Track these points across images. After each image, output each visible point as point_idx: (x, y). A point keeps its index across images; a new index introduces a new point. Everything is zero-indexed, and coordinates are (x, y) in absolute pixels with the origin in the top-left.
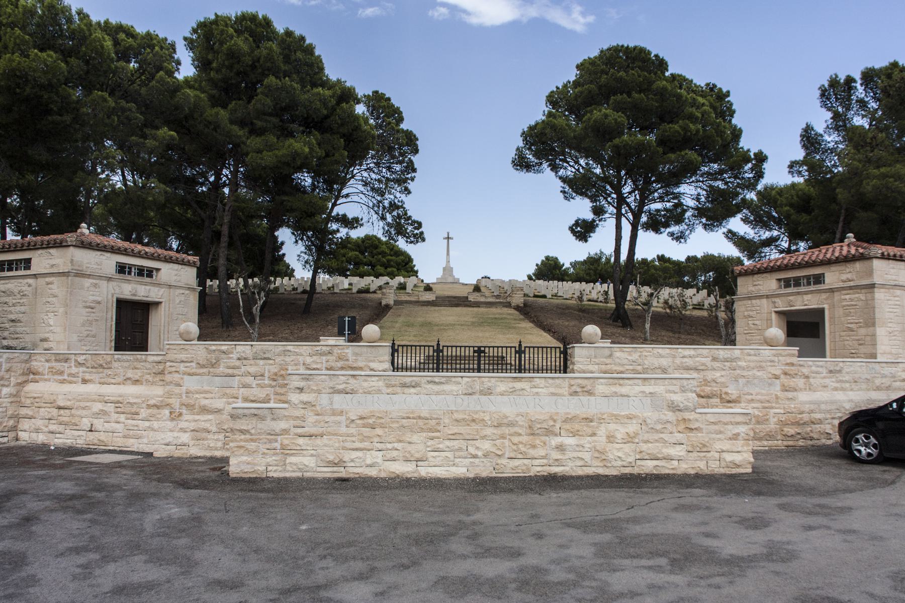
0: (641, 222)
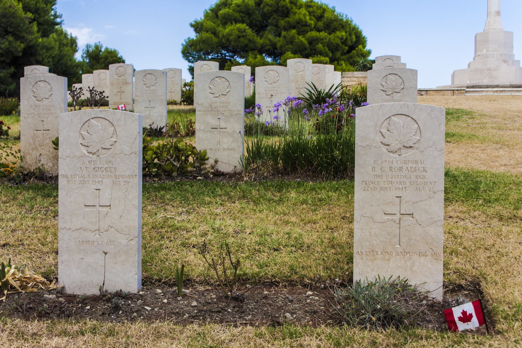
0: (456, 319)
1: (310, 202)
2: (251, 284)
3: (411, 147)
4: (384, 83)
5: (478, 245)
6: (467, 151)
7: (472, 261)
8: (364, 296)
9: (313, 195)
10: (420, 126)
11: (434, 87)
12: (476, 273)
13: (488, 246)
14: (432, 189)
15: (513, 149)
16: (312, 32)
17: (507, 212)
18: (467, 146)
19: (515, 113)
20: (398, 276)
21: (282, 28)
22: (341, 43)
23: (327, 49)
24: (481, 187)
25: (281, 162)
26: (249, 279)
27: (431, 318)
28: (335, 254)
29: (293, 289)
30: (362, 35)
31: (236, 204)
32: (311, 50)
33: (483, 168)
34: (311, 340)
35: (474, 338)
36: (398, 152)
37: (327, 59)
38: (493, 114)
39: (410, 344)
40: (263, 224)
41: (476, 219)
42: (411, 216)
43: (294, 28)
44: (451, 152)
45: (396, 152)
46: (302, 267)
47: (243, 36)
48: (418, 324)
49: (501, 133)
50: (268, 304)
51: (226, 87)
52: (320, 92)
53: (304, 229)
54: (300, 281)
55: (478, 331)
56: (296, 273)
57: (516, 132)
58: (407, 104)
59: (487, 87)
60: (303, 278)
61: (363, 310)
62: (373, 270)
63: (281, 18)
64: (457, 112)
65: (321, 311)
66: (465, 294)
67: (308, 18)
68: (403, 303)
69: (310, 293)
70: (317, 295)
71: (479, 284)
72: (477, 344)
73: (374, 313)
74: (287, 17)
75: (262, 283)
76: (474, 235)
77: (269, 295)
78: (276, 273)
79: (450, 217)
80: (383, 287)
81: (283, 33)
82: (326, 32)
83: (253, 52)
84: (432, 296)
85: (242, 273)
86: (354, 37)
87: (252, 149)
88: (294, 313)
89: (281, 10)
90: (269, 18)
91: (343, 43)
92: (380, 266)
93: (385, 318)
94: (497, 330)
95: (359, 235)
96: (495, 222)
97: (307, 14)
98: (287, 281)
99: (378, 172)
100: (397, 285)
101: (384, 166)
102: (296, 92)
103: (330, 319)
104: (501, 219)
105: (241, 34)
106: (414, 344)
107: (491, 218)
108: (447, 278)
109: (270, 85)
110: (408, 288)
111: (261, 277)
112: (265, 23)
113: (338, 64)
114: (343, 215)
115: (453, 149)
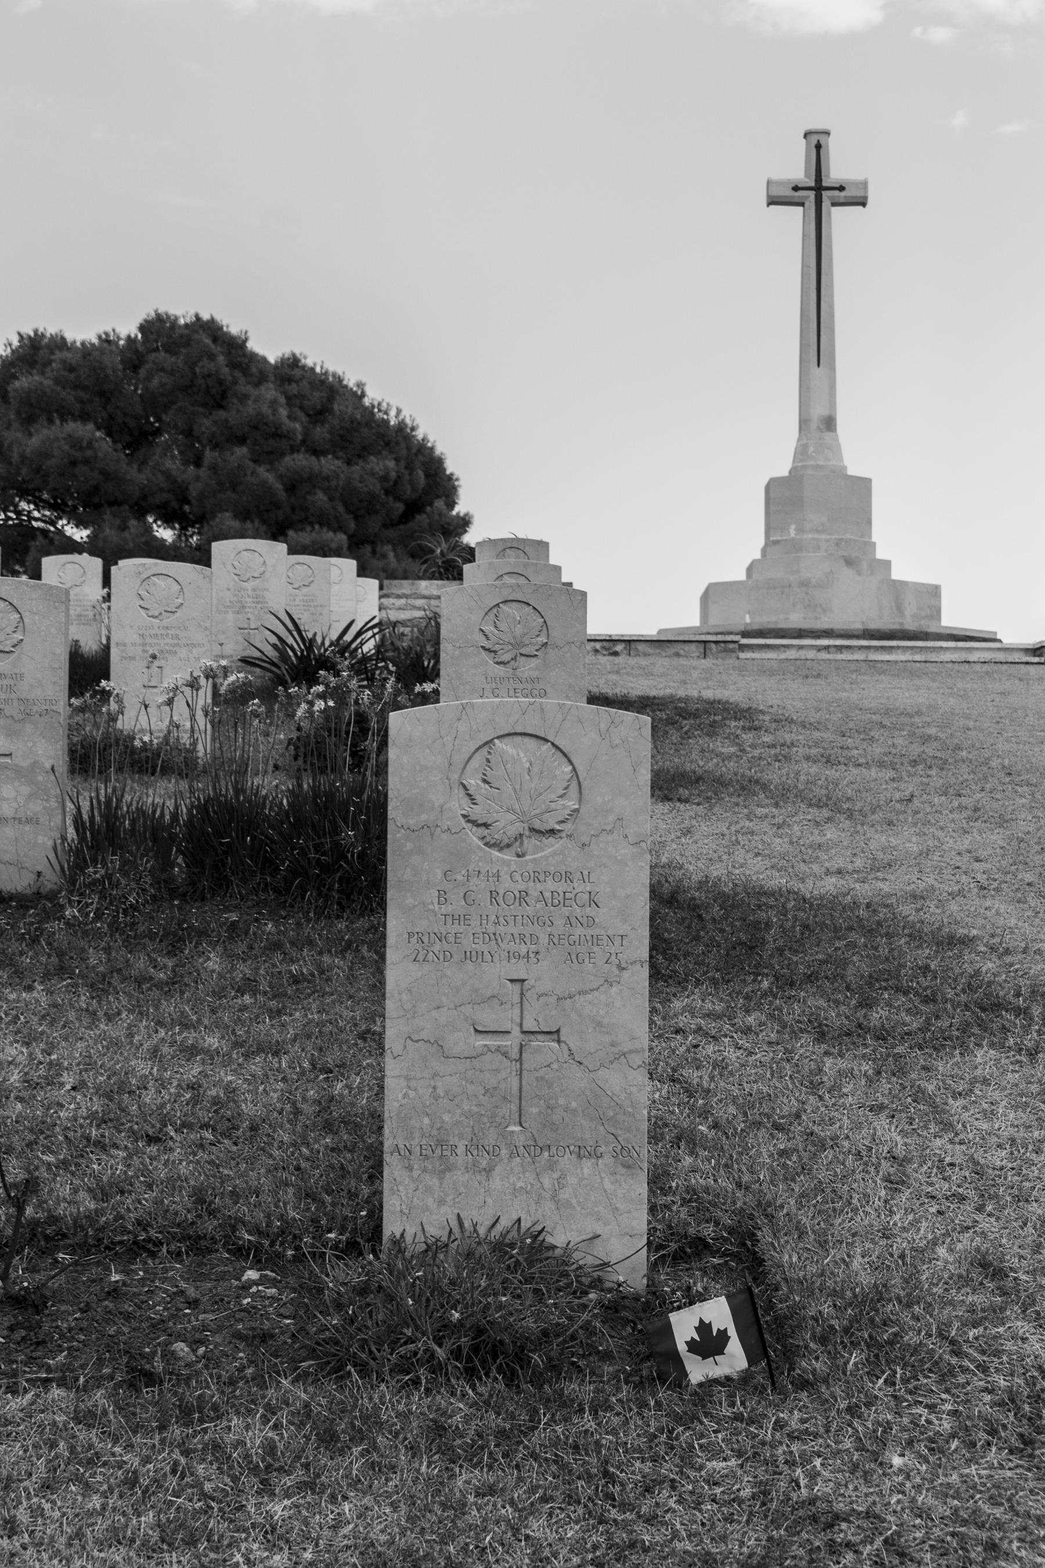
0: (682, 1347)
1: (264, 986)
2: (72, 1250)
3: (552, 832)
4: (489, 628)
5: (754, 1115)
6: (733, 829)
7: (736, 1166)
8: (413, 1285)
9: (274, 966)
10: (581, 770)
11: (650, 630)
12: (745, 1203)
13: (783, 1117)
14: (613, 957)
15: (863, 825)
16: (295, 455)
17: (838, 1015)
18: (735, 813)
19: (873, 717)
20: (515, 1218)
21: (204, 442)
22: (382, 492)
23: (341, 509)
24: (769, 938)
25: (180, 860)
26: (65, 1236)
27: (608, 1343)
28: (333, 1150)
29: (200, 1264)
30: (445, 470)
31: (35, 994)
32: (293, 509)
33: (777, 881)
34: (248, 1427)
35: (732, 1404)
36: (517, 847)
37: (342, 538)
38: (813, 717)
39: (545, 1429)
40: (116, 1057)
41: (752, 1036)
42: (555, 1036)
43: (242, 440)
44: (689, 832)
45: (508, 846)
46: (233, 1193)
47: (87, 461)
48: (574, 1363)
49: (832, 773)
50: (121, 1313)
51: (10, 630)
52: (312, 641)
53: (244, 1071)
54: (225, 1237)
55: (745, 1378)
56: (212, 1213)
57: (873, 772)
58: (541, 704)
59: (800, 634)
60: (234, 1229)
61: (408, 1327)
62: (441, 1202)
63: (201, 409)
64: (711, 711)
65: (283, 1333)
66: (714, 1267)
67: (283, 412)
68: (528, 1303)
69: (252, 1275)
70: (274, 1283)
71: (754, 1235)
72: (742, 1422)
73: (444, 1336)
74: (220, 407)
75: (107, 1248)
76: (745, 1085)
77: (124, 1284)
78: (150, 1214)
79: (677, 1032)
80: (469, 1255)
81: (209, 456)
82: (338, 458)
83: (115, 508)
84: (614, 1278)
85: (41, 1215)
86: (421, 474)
87: (92, 818)
88: (201, 1342)
89: (204, 386)
90: (166, 407)
91: (387, 492)
92: (462, 1189)
93: (475, 1349)
94: (799, 1375)
95: (400, 1096)
96: (805, 1046)
97: (282, 400)
98: (184, 1238)
99: (456, 905)
100: (512, 1246)
101: (473, 888)
102: (240, 639)
103: (310, 1359)
104: (821, 1036)
105: (78, 455)
106: (559, 1429)
107: (794, 1032)
108: (664, 1217)
109: (157, 621)
110: (546, 1255)
111: (102, 1229)
112: (152, 424)
113: (374, 552)
114: (364, 1027)
115: (694, 822)
